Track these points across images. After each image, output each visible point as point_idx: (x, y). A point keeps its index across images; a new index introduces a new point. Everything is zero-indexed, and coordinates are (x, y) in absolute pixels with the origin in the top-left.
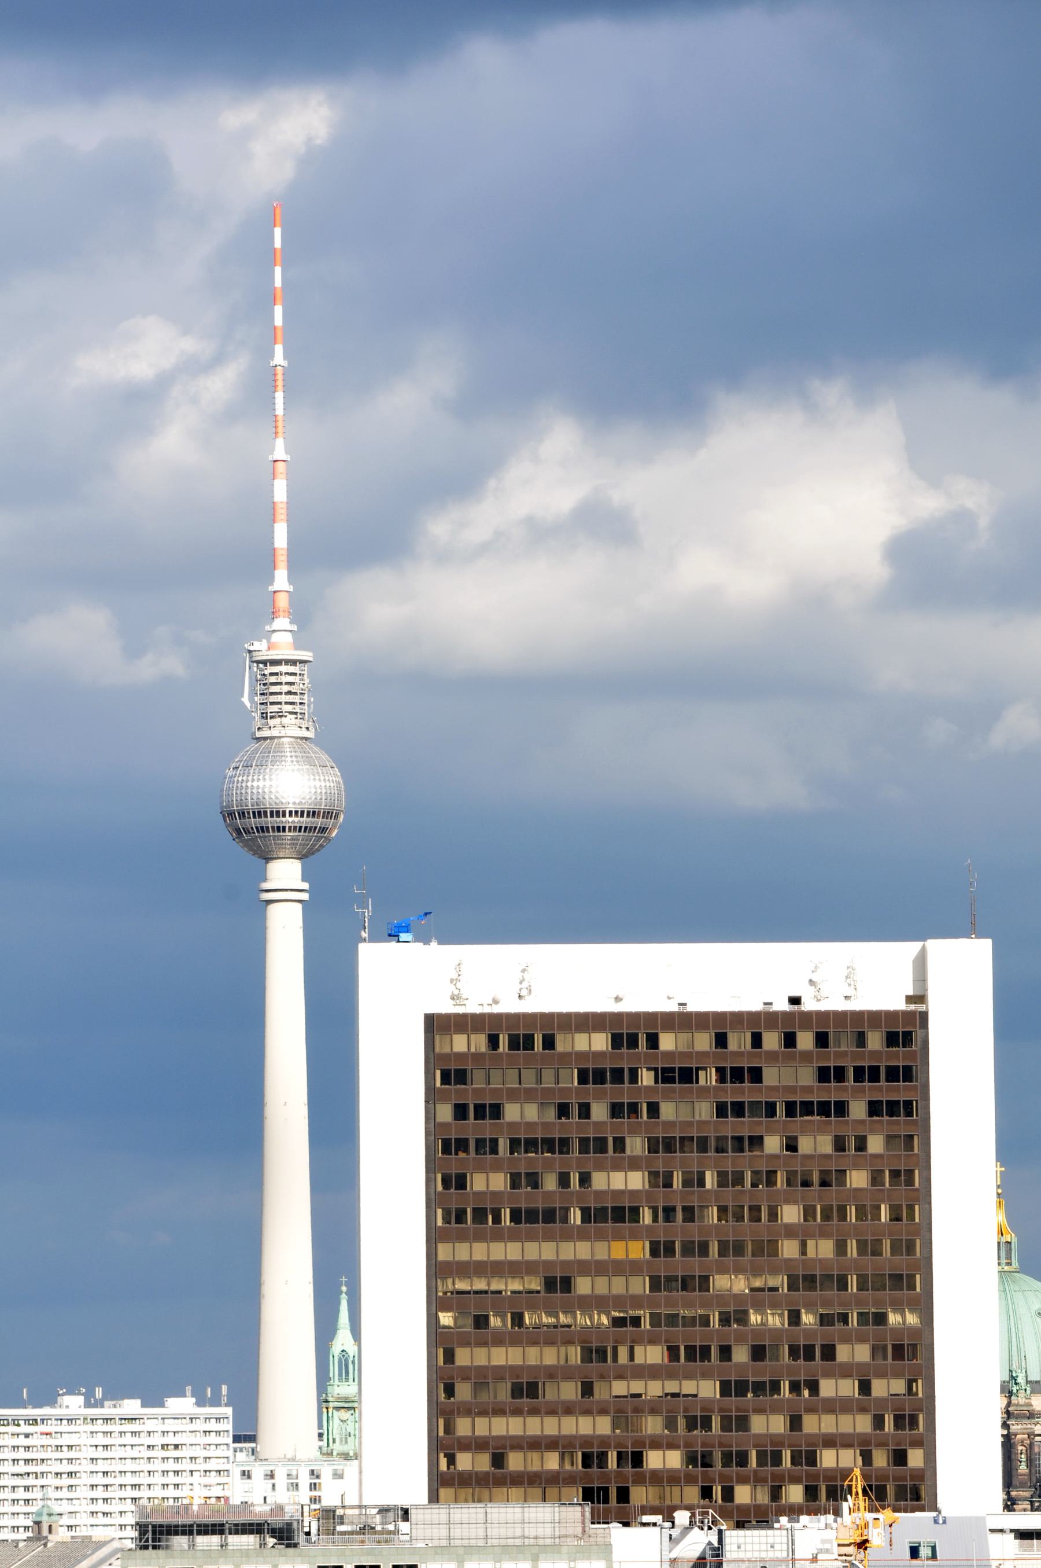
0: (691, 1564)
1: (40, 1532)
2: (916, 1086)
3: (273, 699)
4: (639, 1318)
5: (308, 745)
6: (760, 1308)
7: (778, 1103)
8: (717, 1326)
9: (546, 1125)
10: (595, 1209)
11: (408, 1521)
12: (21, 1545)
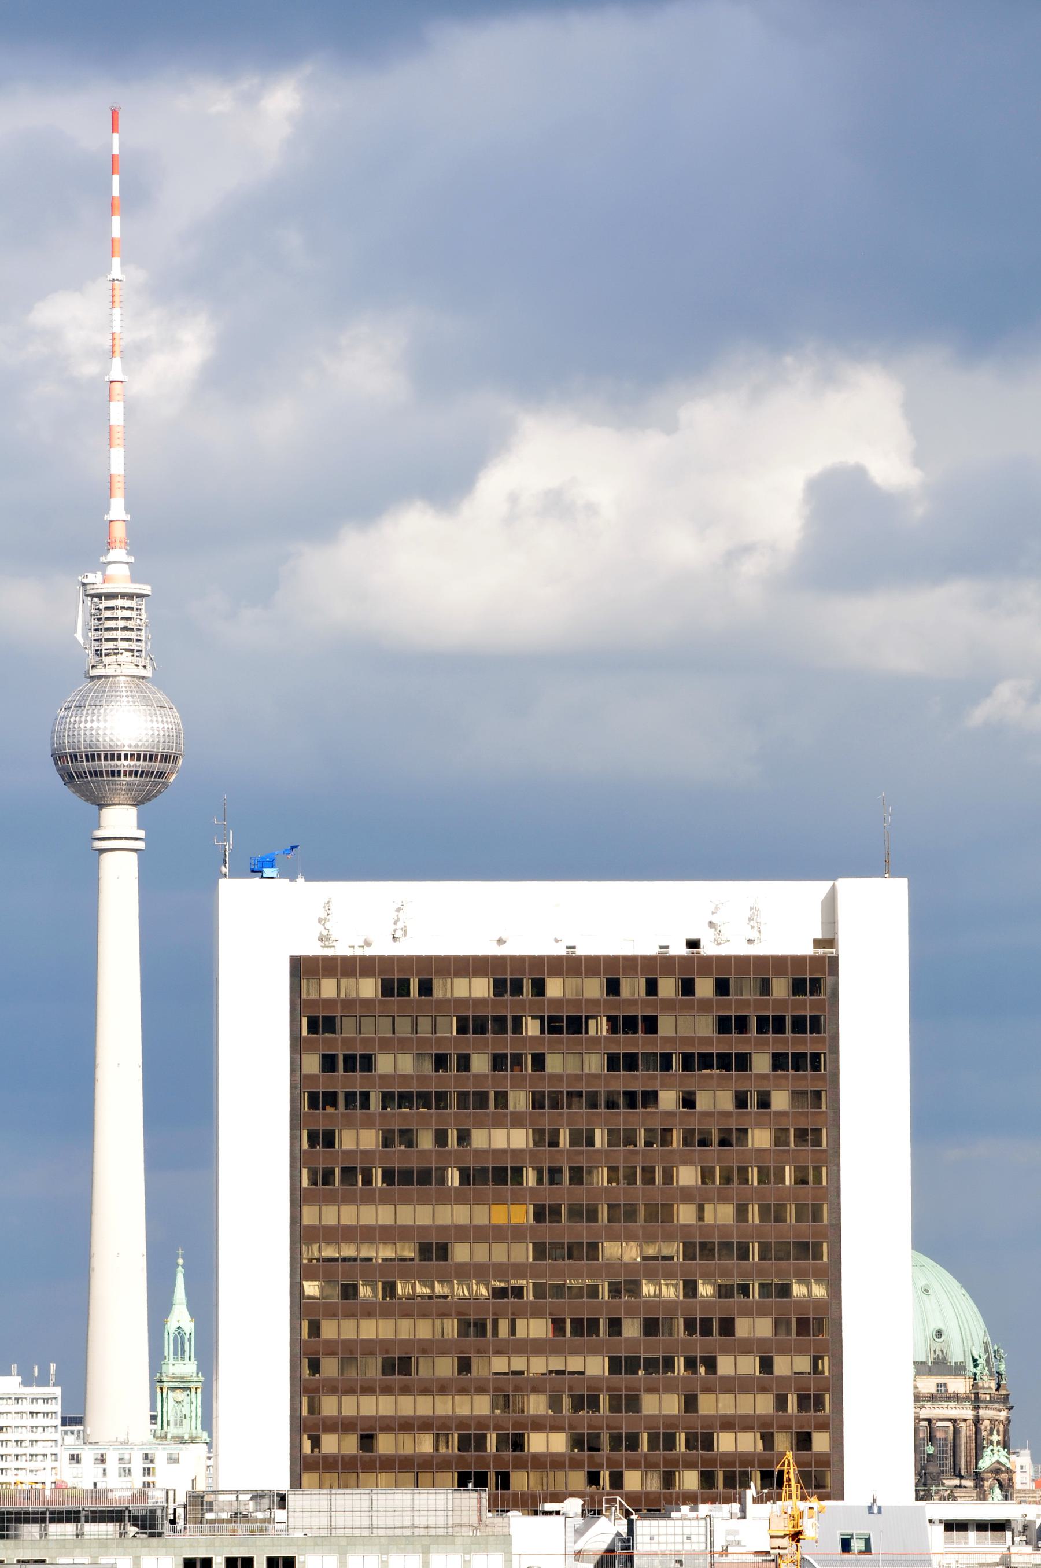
0: (597, 1557)
2: (825, 1037)
4: (521, 1288)
6: (653, 1277)
7: (674, 1056)
8: (606, 1298)
9: (421, 1078)
11: (284, 1508)
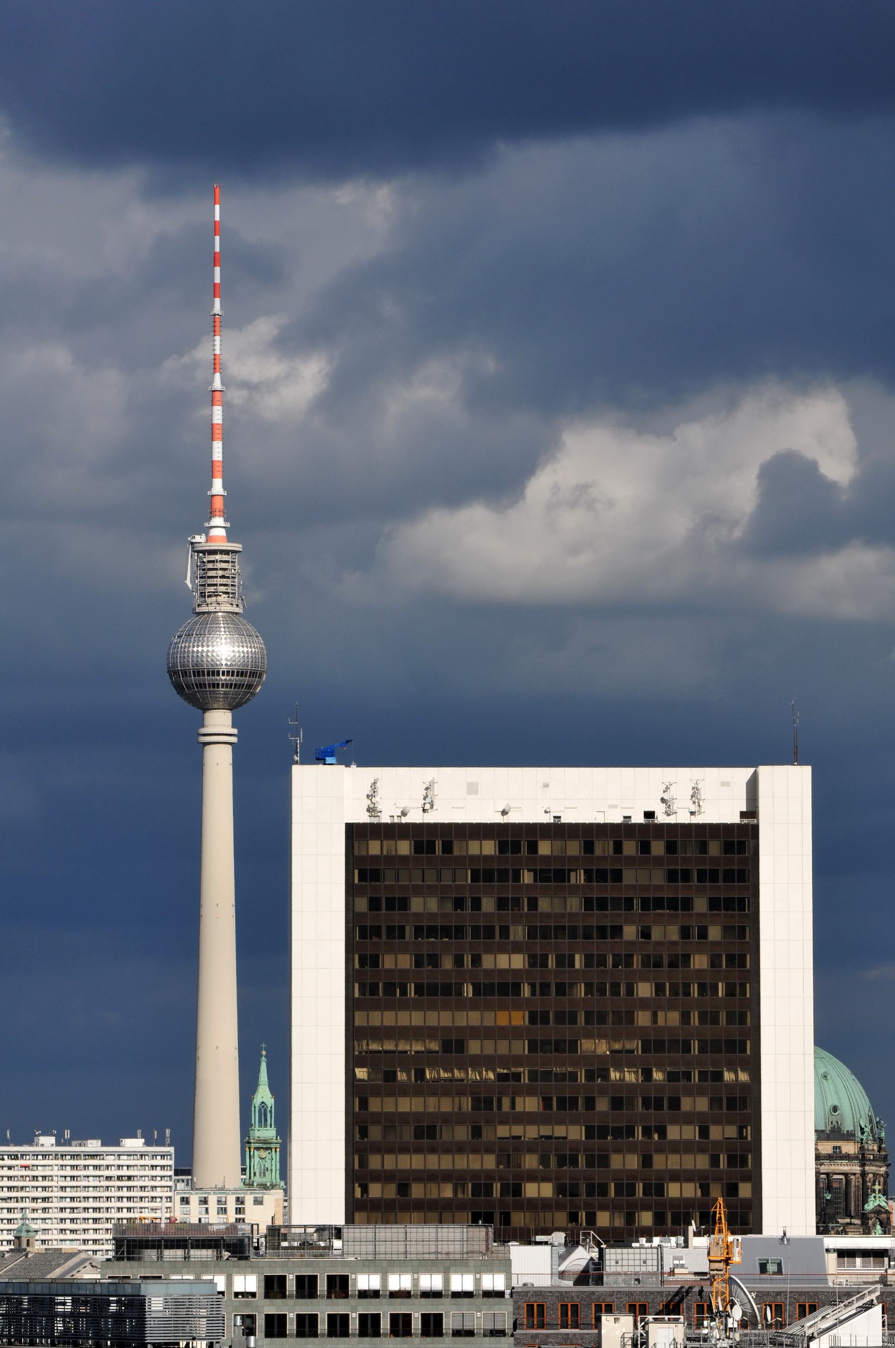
0: (576, 1276)
1: (20, 1245)
3: (210, 581)
5: (237, 619)
6: (619, 1068)
7: (635, 899)
8: (583, 1081)
9: (444, 916)
10: (484, 984)
11: (340, 1239)
12: (7, 1255)
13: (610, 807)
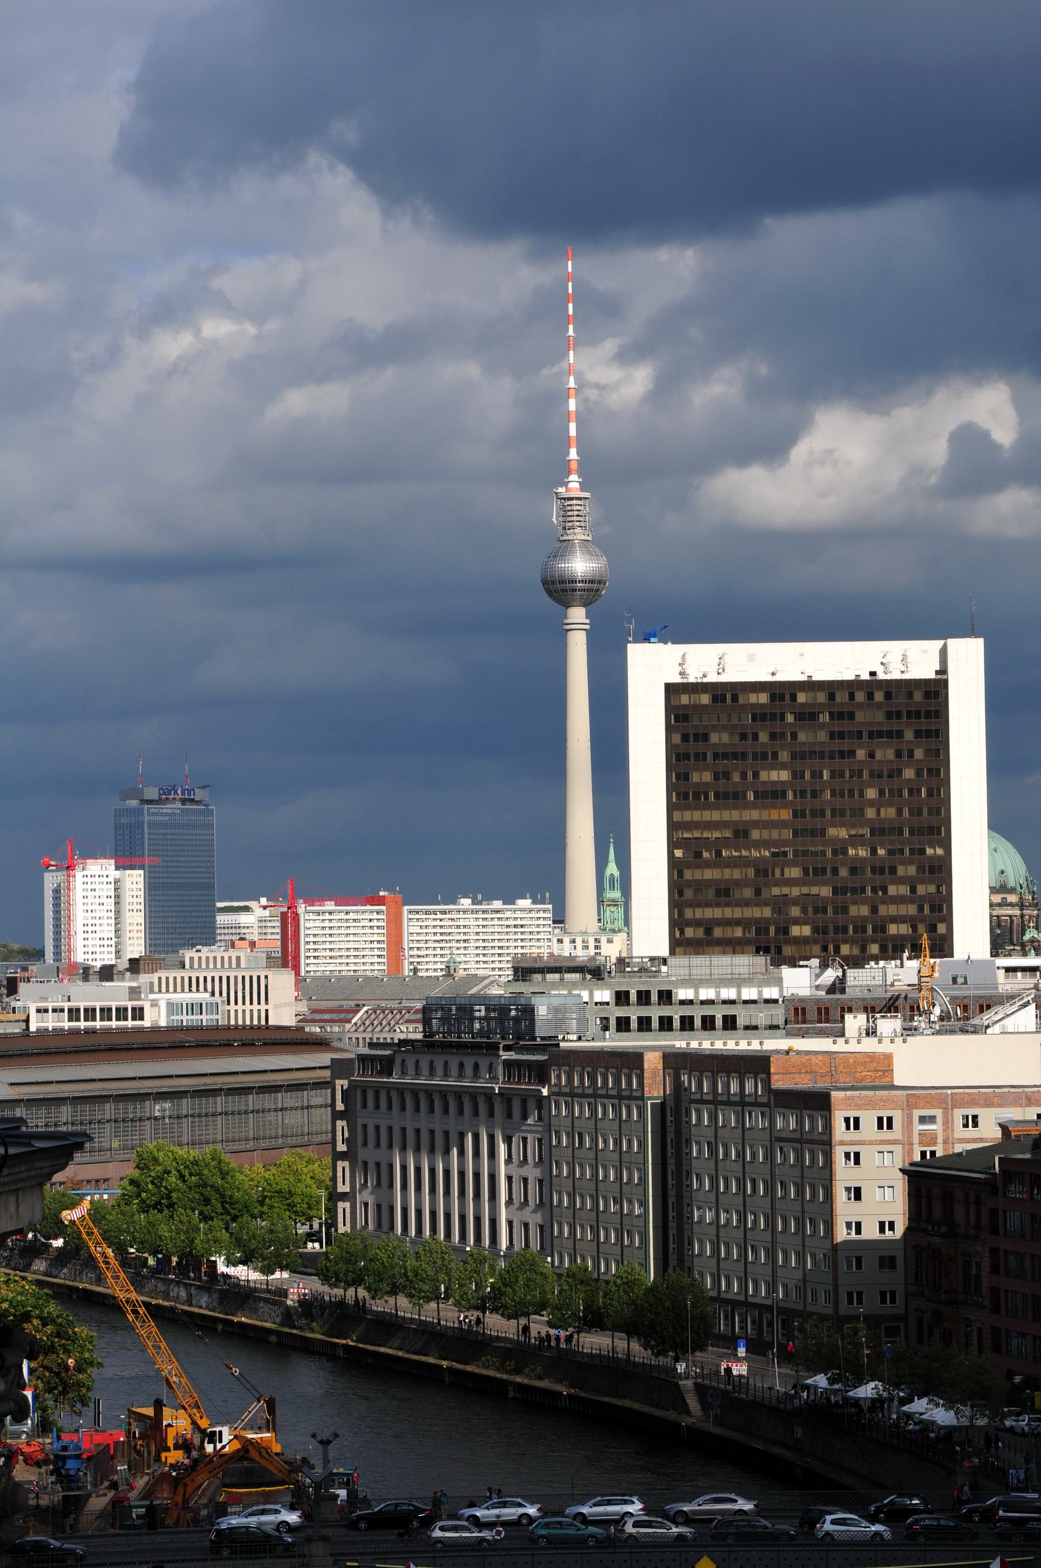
6: (855, 847)
13: (847, 669)
